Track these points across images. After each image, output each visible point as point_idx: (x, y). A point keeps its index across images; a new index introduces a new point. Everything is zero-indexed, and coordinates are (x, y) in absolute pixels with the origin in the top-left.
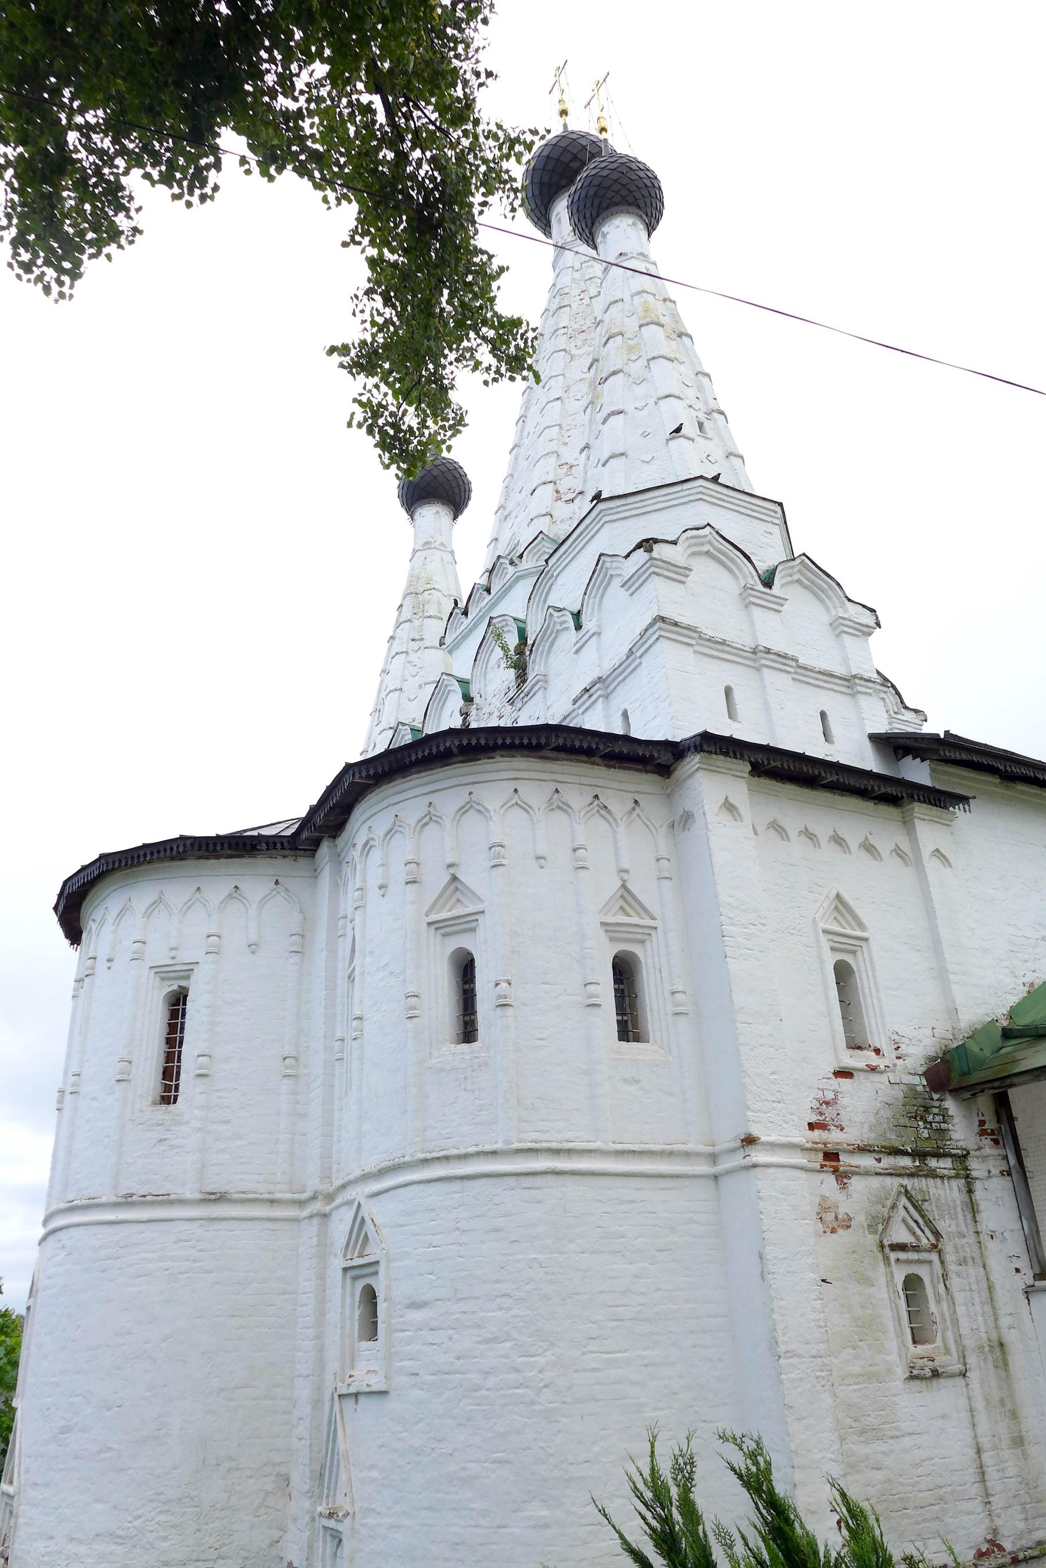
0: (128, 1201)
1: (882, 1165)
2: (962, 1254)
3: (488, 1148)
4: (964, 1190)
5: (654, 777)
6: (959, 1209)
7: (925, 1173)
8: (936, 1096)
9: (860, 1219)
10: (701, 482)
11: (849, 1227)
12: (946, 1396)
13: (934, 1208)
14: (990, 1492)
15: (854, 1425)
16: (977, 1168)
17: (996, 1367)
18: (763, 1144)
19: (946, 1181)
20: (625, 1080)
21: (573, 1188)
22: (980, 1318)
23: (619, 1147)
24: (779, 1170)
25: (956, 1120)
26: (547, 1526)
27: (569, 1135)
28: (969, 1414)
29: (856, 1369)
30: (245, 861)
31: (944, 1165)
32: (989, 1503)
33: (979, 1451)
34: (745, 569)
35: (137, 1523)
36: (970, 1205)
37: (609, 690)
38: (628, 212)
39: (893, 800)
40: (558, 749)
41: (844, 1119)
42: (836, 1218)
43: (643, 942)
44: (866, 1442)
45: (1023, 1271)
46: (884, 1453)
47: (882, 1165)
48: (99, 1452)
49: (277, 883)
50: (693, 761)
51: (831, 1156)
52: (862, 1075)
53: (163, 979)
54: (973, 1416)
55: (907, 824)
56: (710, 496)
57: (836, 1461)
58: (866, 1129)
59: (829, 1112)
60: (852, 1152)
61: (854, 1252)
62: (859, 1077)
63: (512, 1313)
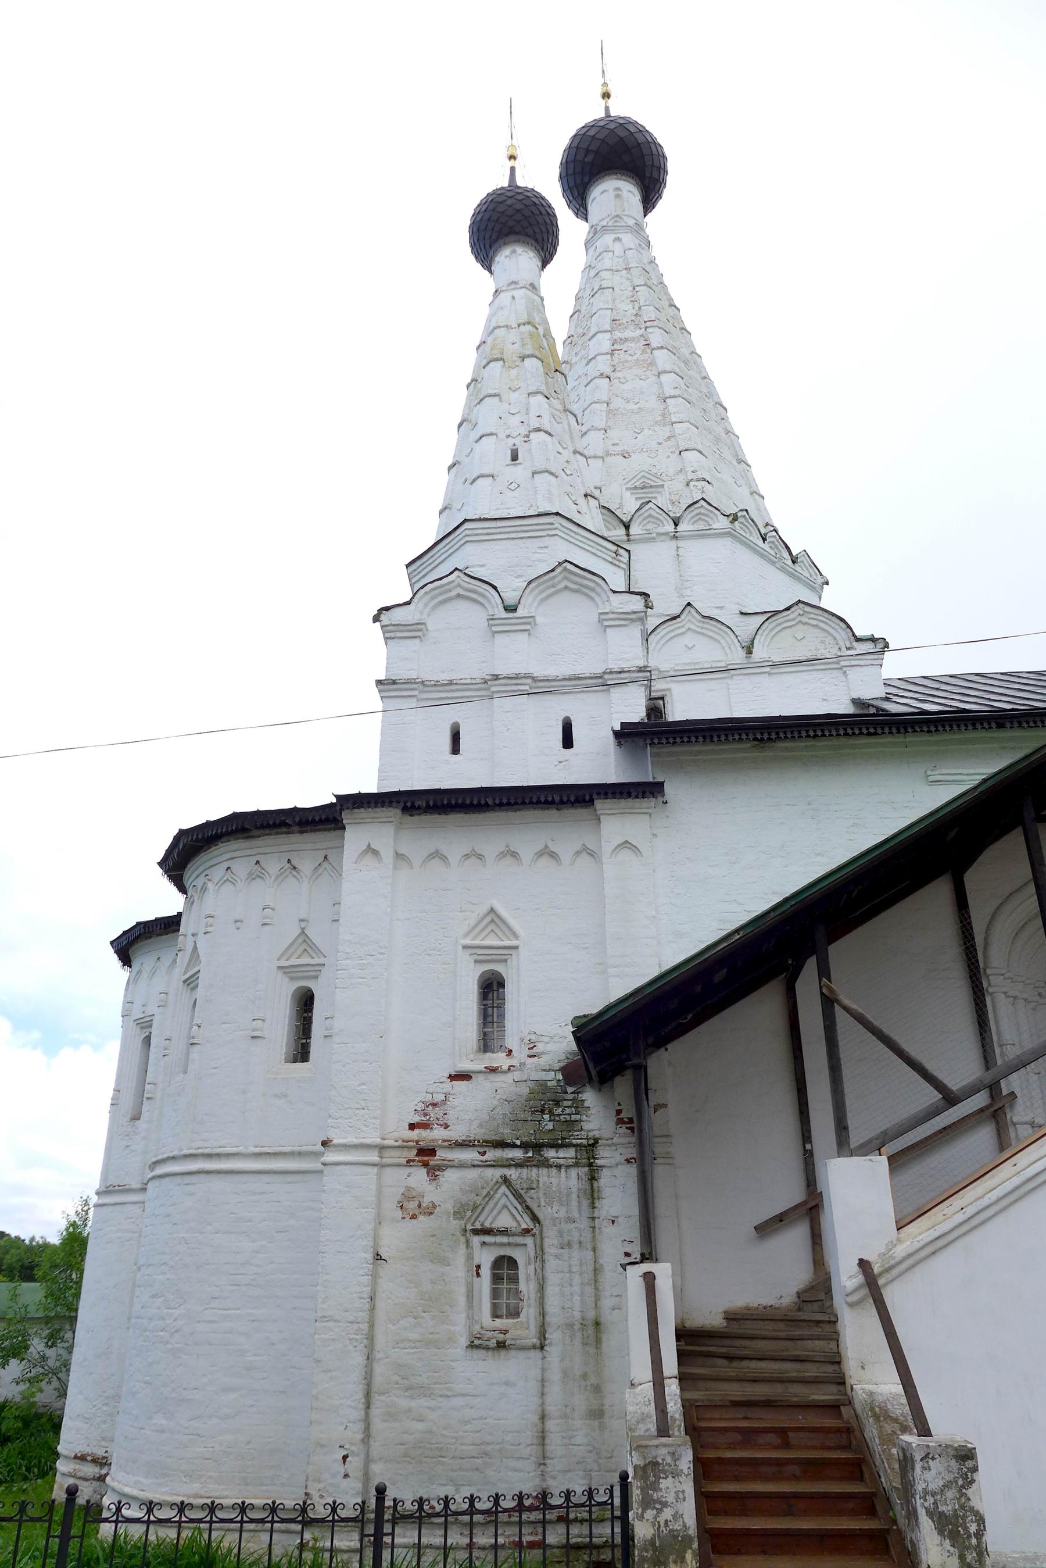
2: (566, 1238)
4: (585, 1178)
6: (574, 1196)
8: (570, 1090)
10: (467, 525)
12: (517, 1368)
13: (541, 1196)
14: (548, 1454)
15: (401, 1382)
16: (605, 1156)
17: (585, 1344)
18: (335, 1146)
19: (563, 1170)
20: (276, 1096)
21: (217, 1184)
22: (577, 1298)
24: (348, 1167)
25: (593, 1111)
26: (163, 1431)
27: (223, 1142)
28: (539, 1384)
29: (413, 1336)
32: (545, 1464)
33: (543, 1417)
34: (493, 601)
36: (589, 1191)
41: (450, 1119)
42: (420, 1206)
44: (412, 1397)
46: (429, 1408)
51: (426, 1152)
52: (481, 1077)
53: (142, 1028)
54: (543, 1386)
56: (477, 535)
57: (355, 1408)
58: (475, 1125)
60: (450, 1147)
62: (478, 1080)
63: (167, 1276)
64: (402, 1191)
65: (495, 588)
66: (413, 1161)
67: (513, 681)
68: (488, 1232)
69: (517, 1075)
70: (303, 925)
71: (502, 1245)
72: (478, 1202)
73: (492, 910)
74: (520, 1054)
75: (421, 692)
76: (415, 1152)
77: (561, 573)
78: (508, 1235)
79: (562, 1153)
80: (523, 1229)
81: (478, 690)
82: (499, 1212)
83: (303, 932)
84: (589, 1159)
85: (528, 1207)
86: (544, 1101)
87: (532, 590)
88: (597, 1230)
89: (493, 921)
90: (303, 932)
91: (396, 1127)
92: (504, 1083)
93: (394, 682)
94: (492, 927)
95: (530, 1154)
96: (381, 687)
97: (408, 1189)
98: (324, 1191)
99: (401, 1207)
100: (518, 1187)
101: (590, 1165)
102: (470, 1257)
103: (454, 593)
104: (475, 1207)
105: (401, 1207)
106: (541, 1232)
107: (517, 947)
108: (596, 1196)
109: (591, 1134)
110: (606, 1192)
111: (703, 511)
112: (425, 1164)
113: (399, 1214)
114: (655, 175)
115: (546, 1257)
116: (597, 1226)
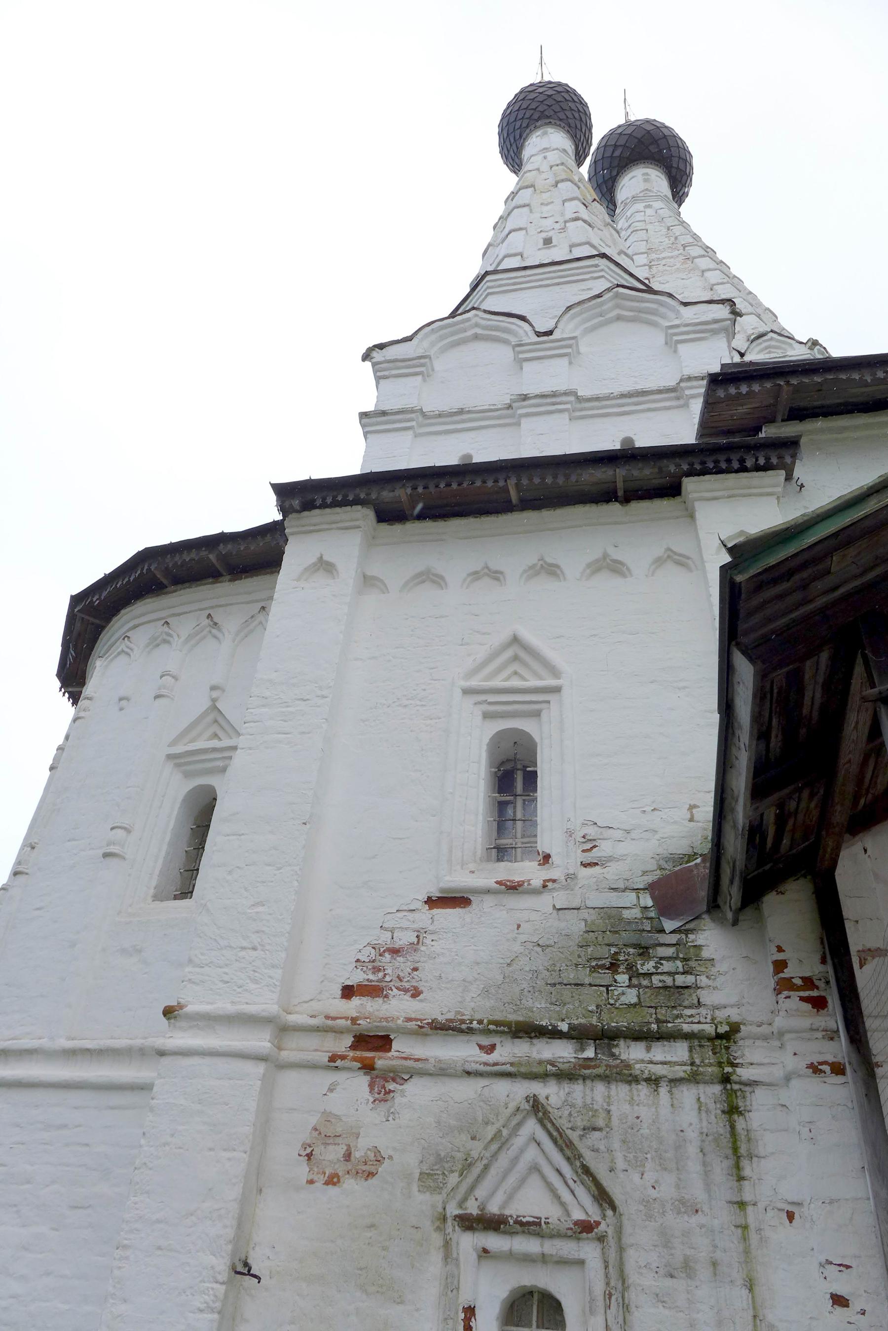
1: (494, 1057)
4: (716, 1109)
6: (692, 1150)
7: (600, 1071)
8: (669, 925)
10: (488, 278)
11: (371, 1175)
13: (616, 1145)
16: (754, 1060)
24: (208, 1060)
34: (521, 332)
36: (726, 1141)
40: (762, 688)
41: (426, 977)
42: (348, 1156)
45: (857, 1305)
47: (494, 1057)
51: (372, 1042)
59: (392, 967)
61: (372, 1226)
62: (482, 906)
64: (313, 1120)
65: (523, 318)
66: (343, 1058)
67: (549, 400)
68: (493, 1224)
69: (561, 898)
70: (215, 694)
71: (527, 1259)
72: (475, 1154)
73: (515, 640)
74: (566, 858)
75: (421, 426)
76: (349, 1040)
77: (611, 299)
78: (540, 1235)
79: (660, 1052)
80: (576, 1223)
81: (499, 418)
82: (523, 1181)
83: (214, 708)
84: (720, 1064)
85: (587, 1171)
86: (618, 949)
87: (572, 318)
88: (754, 1238)
89: (516, 658)
90: (214, 708)
91: (317, 995)
92: (535, 914)
93: (384, 413)
94: (515, 667)
95: (590, 1053)
96: (365, 421)
97: (328, 1117)
98: (152, 1109)
99: (309, 1156)
100: (564, 1124)
101: (726, 1079)
102: (451, 1285)
103: (470, 333)
104: (468, 1165)
105: (309, 1156)
106: (619, 1230)
107: (557, 690)
108: (743, 1150)
109: (721, 1015)
110: (767, 1142)
111: (773, 343)
112: (368, 1067)
113: (303, 1171)
114: (682, 166)
115: (632, 1296)
116: (751, 1220)
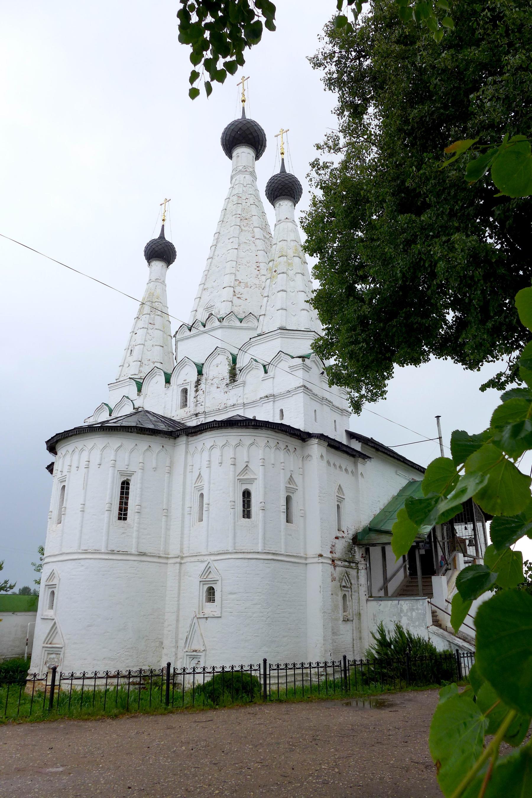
0: (112, 552)
3: (256, 551)
5: (300, 441)
9: (337, 578)
10: (313, 333)
23: (287, 554)
26: (267, 652)
27: (276, 549)
30: (153, 437)
31: (353, 565)
33: (353, 640)
35: (118, 655)
37: (276, 400)
38: (290, 200)
39: (353, 456)
43: (293, 493)
48: (105, 633)
49: (163, 447)
50: (315, 441)
55: (355, 464)
